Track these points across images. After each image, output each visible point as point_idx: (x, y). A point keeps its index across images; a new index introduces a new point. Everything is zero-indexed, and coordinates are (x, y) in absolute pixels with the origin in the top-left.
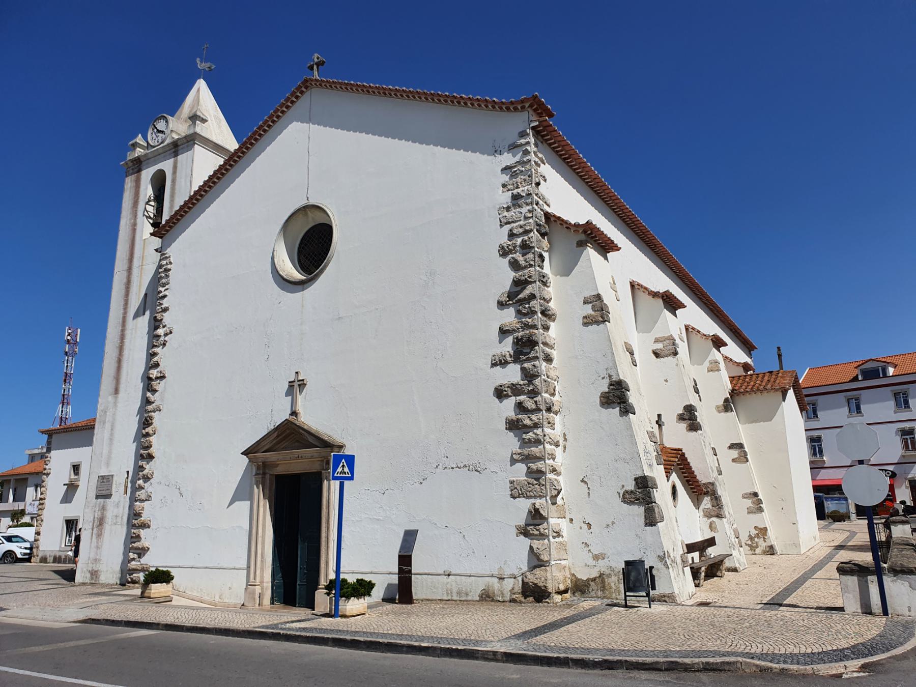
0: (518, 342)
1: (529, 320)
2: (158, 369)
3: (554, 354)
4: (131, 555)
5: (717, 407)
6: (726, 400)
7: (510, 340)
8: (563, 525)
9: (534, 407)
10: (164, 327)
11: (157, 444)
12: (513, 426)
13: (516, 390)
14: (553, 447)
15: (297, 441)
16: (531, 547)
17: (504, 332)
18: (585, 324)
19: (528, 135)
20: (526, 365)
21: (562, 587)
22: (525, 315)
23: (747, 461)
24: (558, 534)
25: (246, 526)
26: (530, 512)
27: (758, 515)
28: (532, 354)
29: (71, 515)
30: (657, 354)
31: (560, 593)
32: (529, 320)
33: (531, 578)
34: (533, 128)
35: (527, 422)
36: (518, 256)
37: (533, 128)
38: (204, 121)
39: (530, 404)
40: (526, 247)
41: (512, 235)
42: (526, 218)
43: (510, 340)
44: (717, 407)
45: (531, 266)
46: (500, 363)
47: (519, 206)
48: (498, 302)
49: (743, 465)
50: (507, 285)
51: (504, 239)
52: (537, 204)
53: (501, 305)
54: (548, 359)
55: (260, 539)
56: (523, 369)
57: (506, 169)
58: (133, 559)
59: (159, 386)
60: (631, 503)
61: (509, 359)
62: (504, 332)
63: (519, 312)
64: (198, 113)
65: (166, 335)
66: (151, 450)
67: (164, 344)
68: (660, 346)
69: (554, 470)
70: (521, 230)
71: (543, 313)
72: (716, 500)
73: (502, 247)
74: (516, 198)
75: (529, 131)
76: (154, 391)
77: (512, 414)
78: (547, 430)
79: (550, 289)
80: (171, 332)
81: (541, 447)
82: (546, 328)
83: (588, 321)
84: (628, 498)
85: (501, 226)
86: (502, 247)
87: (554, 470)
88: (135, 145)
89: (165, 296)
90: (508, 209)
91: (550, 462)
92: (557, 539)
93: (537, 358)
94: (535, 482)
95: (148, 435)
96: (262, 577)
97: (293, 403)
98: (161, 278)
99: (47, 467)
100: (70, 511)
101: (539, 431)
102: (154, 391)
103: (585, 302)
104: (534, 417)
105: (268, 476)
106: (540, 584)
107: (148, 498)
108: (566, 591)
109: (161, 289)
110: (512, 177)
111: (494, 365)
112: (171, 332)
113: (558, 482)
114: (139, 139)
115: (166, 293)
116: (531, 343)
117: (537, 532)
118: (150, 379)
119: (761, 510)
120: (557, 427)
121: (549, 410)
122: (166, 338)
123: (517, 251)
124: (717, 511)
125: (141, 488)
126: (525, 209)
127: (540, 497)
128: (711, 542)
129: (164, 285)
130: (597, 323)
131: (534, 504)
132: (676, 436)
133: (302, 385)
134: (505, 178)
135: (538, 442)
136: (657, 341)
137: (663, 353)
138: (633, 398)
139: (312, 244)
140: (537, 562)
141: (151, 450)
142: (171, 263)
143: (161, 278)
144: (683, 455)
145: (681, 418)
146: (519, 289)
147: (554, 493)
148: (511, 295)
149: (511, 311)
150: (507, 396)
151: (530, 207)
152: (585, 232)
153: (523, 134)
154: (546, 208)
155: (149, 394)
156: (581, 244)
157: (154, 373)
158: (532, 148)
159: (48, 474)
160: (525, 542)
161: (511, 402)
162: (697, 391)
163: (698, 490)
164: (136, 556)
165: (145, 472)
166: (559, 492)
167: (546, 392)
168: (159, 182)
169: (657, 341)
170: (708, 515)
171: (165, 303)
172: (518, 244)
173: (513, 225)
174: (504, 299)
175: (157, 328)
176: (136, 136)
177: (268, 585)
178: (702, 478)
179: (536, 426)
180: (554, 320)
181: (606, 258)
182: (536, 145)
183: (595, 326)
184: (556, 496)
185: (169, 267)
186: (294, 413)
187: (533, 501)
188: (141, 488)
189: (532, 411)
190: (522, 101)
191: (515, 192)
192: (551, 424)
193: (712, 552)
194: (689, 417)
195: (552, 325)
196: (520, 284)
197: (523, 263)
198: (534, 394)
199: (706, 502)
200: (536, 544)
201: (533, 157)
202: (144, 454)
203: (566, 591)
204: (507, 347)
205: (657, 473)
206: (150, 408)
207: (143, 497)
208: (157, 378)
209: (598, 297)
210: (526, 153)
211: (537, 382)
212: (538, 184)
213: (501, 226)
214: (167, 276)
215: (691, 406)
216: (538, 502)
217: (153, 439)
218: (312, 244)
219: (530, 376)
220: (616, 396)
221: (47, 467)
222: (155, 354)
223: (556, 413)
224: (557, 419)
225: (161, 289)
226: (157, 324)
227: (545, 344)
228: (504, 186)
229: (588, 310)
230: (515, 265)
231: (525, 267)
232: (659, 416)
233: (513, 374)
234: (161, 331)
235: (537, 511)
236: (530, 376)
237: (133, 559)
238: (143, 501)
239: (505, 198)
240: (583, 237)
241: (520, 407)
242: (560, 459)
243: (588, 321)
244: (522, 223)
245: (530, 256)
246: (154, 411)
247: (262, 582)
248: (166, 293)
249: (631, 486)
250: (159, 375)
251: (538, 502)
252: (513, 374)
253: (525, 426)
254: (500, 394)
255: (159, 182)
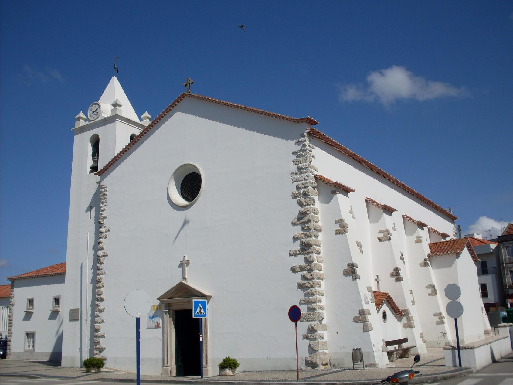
0: (302, 244)
1: (308, 233)
2: (103, 251)
3: (321, 249)
4: (95, 352)
5: (420, 264)
6: (425, 260)
7: (298, 242)
8: (325, 333)
9: (311, 277)
10: (105, 227)
11: (105, 292)
12: (301, 286)
13: (302, 269)
14: (320, 296)
15: (186, 293)
16: (310, 345)
17: (295, 239)
18: (336, 234)
19: (305, 136)
20: (306, 256)
21: (324, 363)
22: (306, 230)
23: (436, 294)
24: (322, 338)
25: (162, 338)
26: (309, 328)
27: (441, 326)
28: (310, 250)
29: (30, 330)
30: (380, 240)
31: (324, 365)
32: (308, 233)
33: (310, 359)
34: (308, 133)
35: (307, 285)
36: (302, 199)
37: (308, 133)
38: (120, 106)
39: (308, 276)
40: (305, 195)
41: (298, 188)
42: (305, 180)
43: (298, 242)
44: (420, 264)
45: (308, 205)
46: (294, 254)
47: (302, 173)
48: (292, 223)
49: (434, 297)
50: (296, 214)
51: (295, 190)
52: (311, 172)
53: (294, 224)
54: (318, 253)
55: (169, 344)
56: (305, 258)
57: (294, 153)
58: (97, 354)
59: (105, 260)
60: (357, 322)
61: (298, 253)
62: (295, 239)
63: (303, 229)
64: (118, 102)
65: (106, 232)
66: (102, 296)
67: (106, 237)
68: (381, 235)
69: (321, 308)
70: (303, 186)
71: (315, 229)
72: (409, 319)
73: (293, 194)
74: (300, 169)
75: (306, 134)
76: (101, 263)
77: (300, 281)
78: (317, 289)
79: (319, 216)
80: (109, 230)
81: (314, 297)
82: (317, 237)
83: (338, 232)
84: (356, 320)
85: (293, 183)
86: (293, 194)
87: (321, 308)
88: (80, 118)
89: (103, 210)
90: (296, 174)
91: (319, 304)
92: (322, 340)
93: (312, 252)
94: (312, 313)
95: (99, 287)
96: (171, 362)
97: (184, 272)
98: (102, 199)
99: (12, 301)
100: (29, 326)
101: (313, 289)
102: (101, 263)
103: (336, 222)
104: (311, 282)
105: (171, 311)
106: (314, 361)
107: (103, 322)
108: (327, 364)
109: (101, 205)
110: (297, 157)
111: (290, 255)
112: (109, 230)
113: (323, 314)
114: (81, 114)
115: (105, 208)
116: (309, 245)
117: (312, 337)
118: (99, 257)
119: (443, 323)
120: (323, 286)
121: (318, 278)
122: (107, 234)
123: (301, 196)
124: (409, 325)
125: (98, 316)
126: (304, 175)
127: (314, 321)
128: (405, 340)
129: (103, 203)
130: (342, 233)
131: (311, 324)
132: (387, 286)
133: (188, 263)
134: (294, 157)
135: (313, 294)
136: (380, 232)
137: (383, 239)
138: (358, 271)
139: (190, 184)
140: (312, 350)
141: (102, 296)
142: (107, 191)
143: (102, 199)
144: (389, 296)
145: (392, 275)
146: (302, 216)
147: (321, 319)
148: (299, 219)
149: (299, 227)
150: (298, 272)
151: (307, 174)
152: (335, 186)
153: (303, 136)
154: (316, 173)
155: (98, 265)
156: (334, 193)
157: (100, 253)
158: (307, 143)
159: (13, 305)
160: (307, 342)
161: (299, 274)
162: (402, 259)
163: (399, 313)
164: (98, 352)
165: (100, 308)
166: (323, 318)
167: (317, 269)
168: (96, 143)
169: (380, 232)
170: (405, 326)
171: (105, 214)
172: (302, 192)
173: (299, 183)
174: (295, 221)
175: (100, 227)
176: (80, 112)
177: (174, 366)
178: (400, 307)
179: (312, 286)
180: (321, 231)
181: (347, 196)
182: (310, 141)
183: (341, 235)
184: (322, 320)
185: (106, 193)
186: (184, 278)
187: (310, 323)
188: (98, 316)
189: (310, 280)
190: (302, 119)
191: (300, 165)
192: (319, 285)
193: (405, 345)
194: (397, 275)
195: (320, 234)
196: (303, 214)
197: (304, 203)
198: (311, 270)
199: (404, 320)
200: (312, 343)
201: (308, 148)
202: (97, 298)
203: (327, 364)
204: (297, 246)
205: (371, 307)
206: (99, 272)
207: (99, 321)
208: (103, 256)
209: (342, 220)
210: (304, 145)
211: (312, 264)
212: (311, 162)
213: (293, 183)
214: (105, 198)
215: (397, 268)
216: (313, 323)
217: (102, 289)
218: (190, 184)
219: (308, 261)
220: (351, 271)
221: (12, 301)
222: (100, 243)
223: (322, 279)
224: (323, 282)
225: (101, 205)
226: (101, 225)
227: (316, 245)
228: (293, 161)
229: (337, 227)
230: (300, 204)
231: (306, 205)
232: (377, 276)
233: (300, 261)
234: (103, 230)
235: (312, 327)
236: (308, 261)
237: (97, 354)
238: (100, 323)
239: (294, 168)
240: (334, 189)
241: (304, 277)
242: (324, 301)
243: (338, 232)
244: (303, 182)
245: (308, 199)
246: (102, 274)
247: (171, 365)
248: (105, 208)
249: (357, 315)
250: (104, 254)
251: (313, 323)
252: (300, 261)
253: (307, 287)
254: (294, 270)
255: (96, 143)
